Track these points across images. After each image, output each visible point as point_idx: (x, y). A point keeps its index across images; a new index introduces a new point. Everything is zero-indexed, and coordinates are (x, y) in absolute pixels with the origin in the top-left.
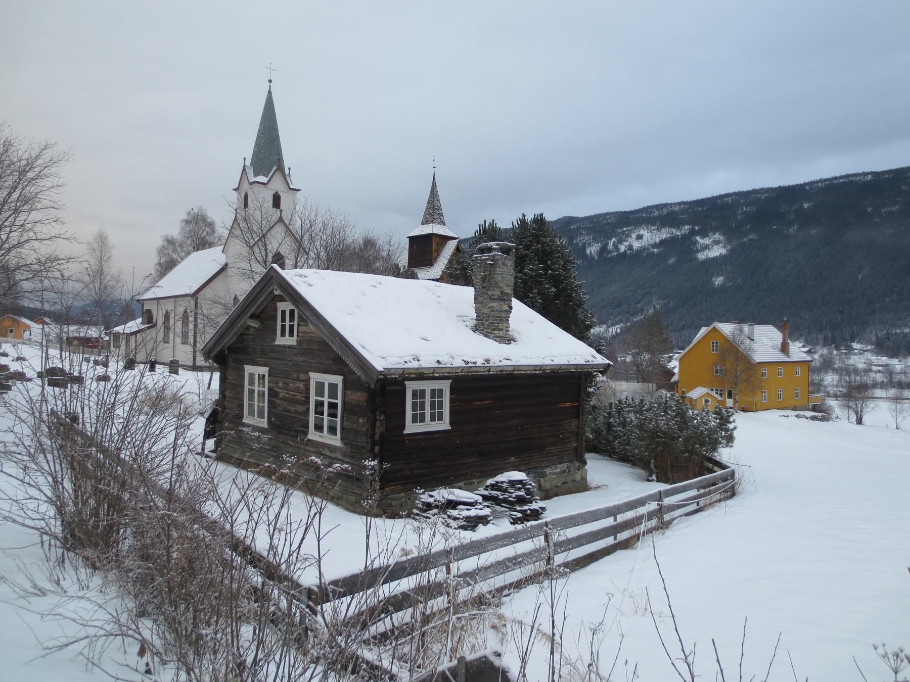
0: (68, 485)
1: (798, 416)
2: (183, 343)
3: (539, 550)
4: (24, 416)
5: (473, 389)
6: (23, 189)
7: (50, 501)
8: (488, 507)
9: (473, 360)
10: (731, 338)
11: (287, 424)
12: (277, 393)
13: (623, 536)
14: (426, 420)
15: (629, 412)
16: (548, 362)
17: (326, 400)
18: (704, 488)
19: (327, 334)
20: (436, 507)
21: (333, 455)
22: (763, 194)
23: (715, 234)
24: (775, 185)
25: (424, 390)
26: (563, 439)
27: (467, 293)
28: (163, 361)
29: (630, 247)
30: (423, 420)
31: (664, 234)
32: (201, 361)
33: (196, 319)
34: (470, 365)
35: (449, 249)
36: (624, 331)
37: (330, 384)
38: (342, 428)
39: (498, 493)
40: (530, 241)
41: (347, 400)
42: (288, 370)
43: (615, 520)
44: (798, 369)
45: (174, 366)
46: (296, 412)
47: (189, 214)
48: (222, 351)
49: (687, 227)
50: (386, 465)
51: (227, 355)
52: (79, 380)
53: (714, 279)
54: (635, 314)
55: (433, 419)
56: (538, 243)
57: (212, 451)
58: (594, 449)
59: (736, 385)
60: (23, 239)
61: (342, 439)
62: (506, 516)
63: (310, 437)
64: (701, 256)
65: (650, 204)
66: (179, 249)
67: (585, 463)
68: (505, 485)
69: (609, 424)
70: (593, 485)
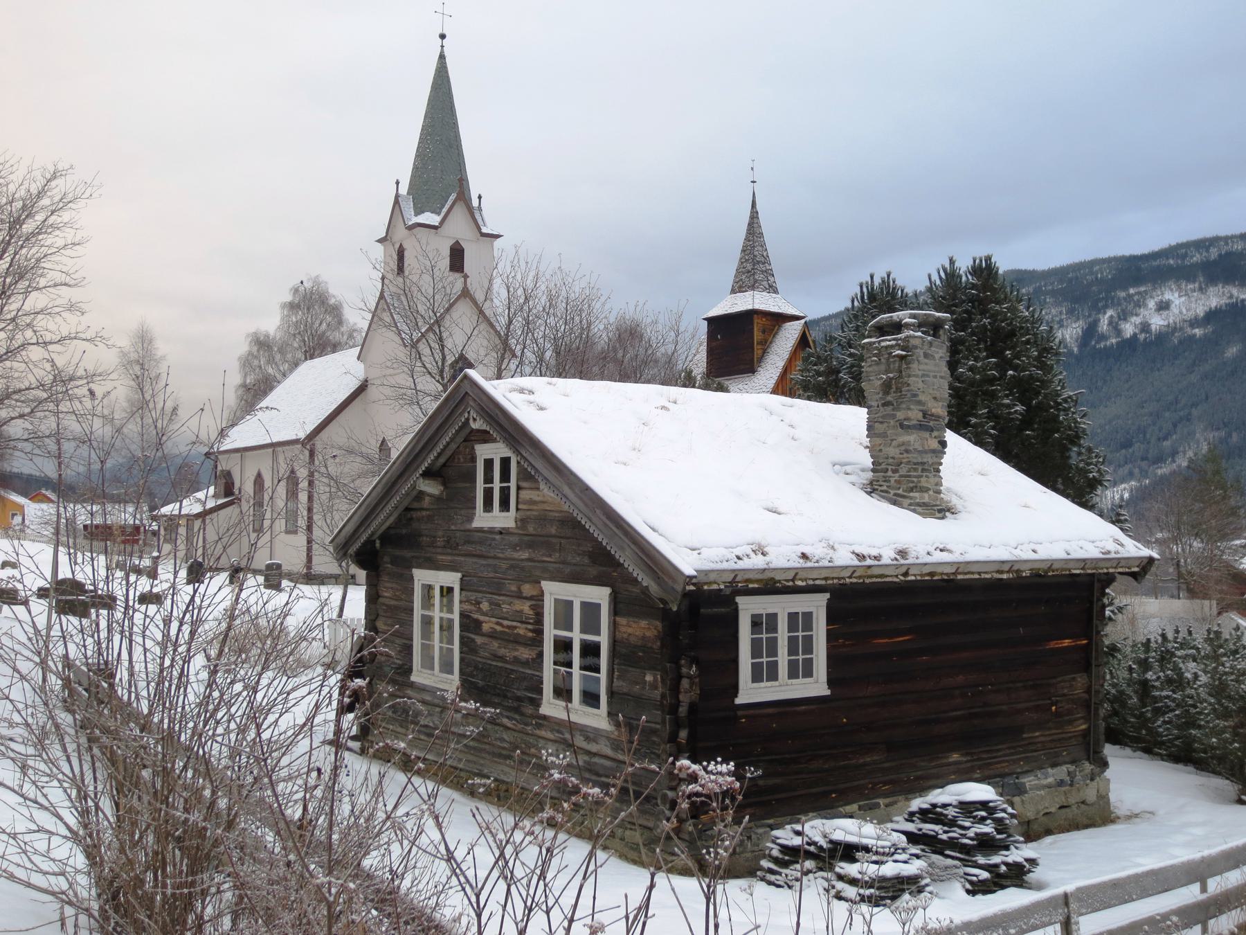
0: (106, 805)
2: (287, 532)
4: (24, 666)
5: (875, 611)
6: (16, 253)
7: (74, 837)
8: (918, 857)
9: (874, 552)
11: (500, 680)
12: (478, 624)
14: (784, 675)
15: (1185, 658)
16: (1026, 554)
17: (577, 636)
20: (809, 855)
21: (593, 748)
25: (775, 615)
26: (1057, 714)
27: (847, 423)
29: (1145, 327)
30: (773, 676)
31: (1215, 298)
32: (325, 562)
34: (869, 562)
36: (1140, 497)
38: (611, 694)
39: (937, 828)
40: (966, 311)
42: (498, 575)
43: (1204, 889)
46: (516, 661)
47: (296, 291)
48: (370, 542)
50: (751, 772)
51: (379, 552)
52: (108, 602)
54: (1159, 460)
55: (793, 674)
56: (983, 313)
57: (354, 738)
58: (1115, 737)
60: (16, 344)
61: (609, 714)
62: (955, 876)
63: (545, 710)
65: (1183, 239)
66: (278, 357)
67: (1105, 765)
68: (951, 812)
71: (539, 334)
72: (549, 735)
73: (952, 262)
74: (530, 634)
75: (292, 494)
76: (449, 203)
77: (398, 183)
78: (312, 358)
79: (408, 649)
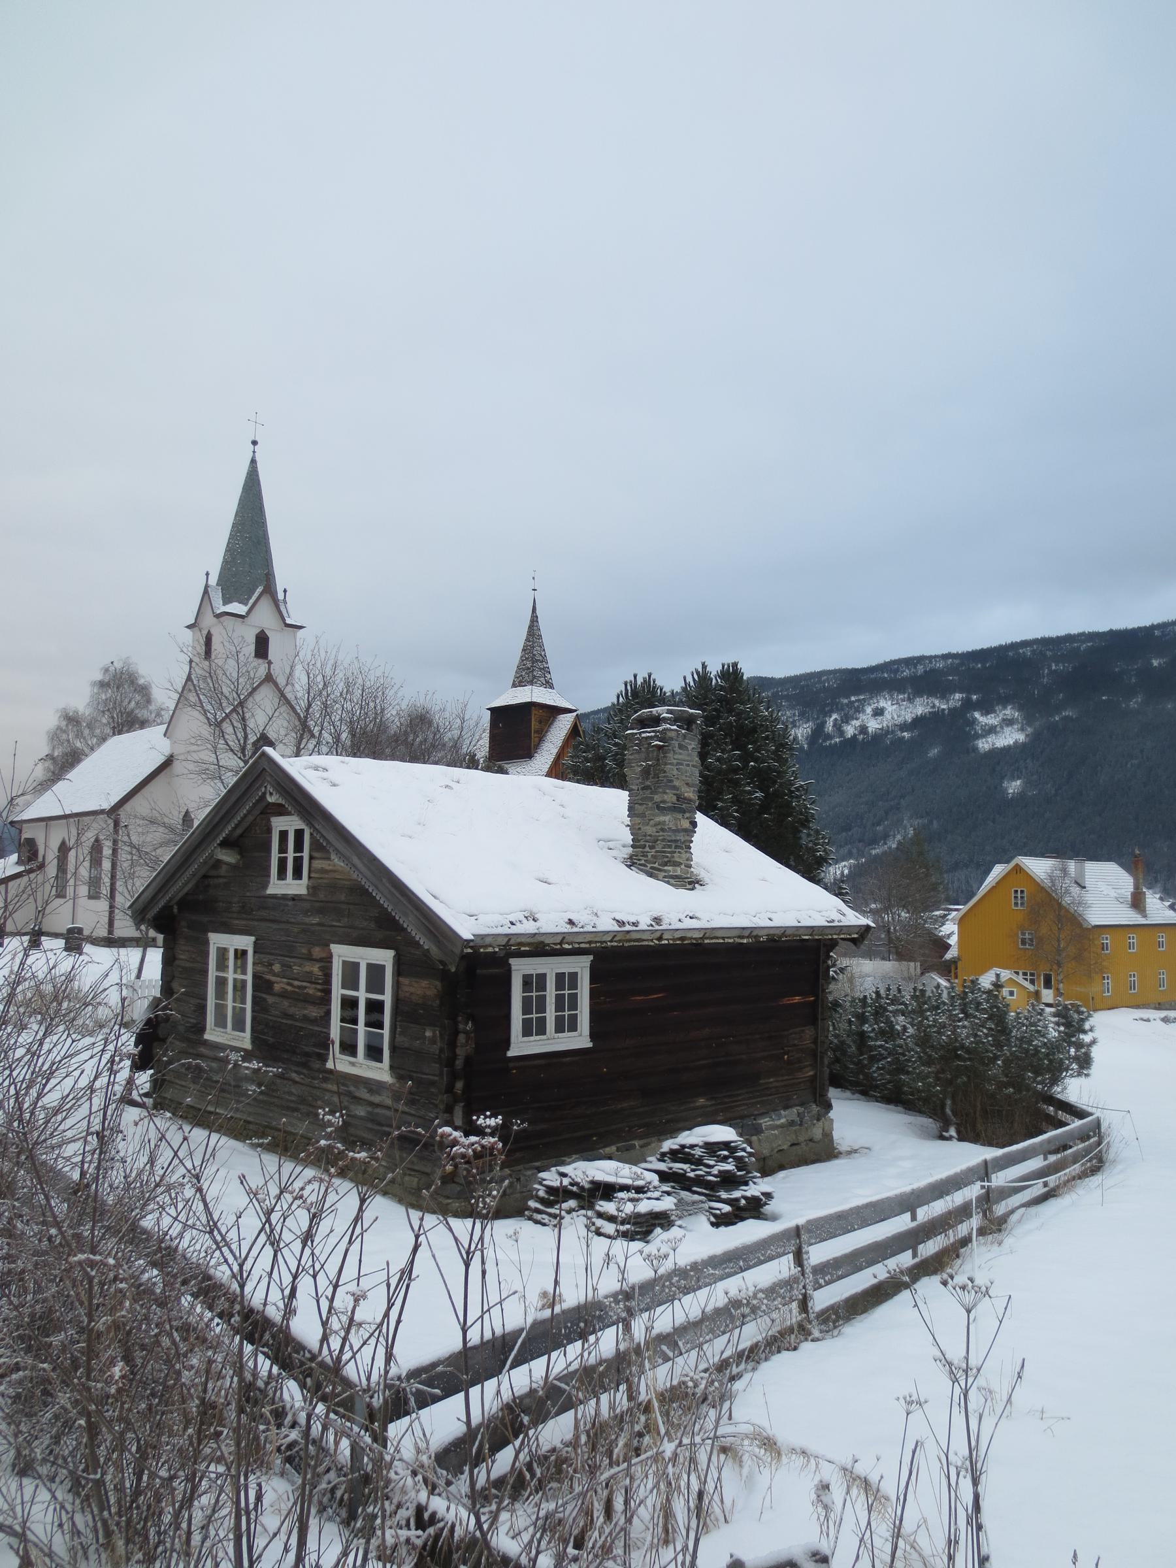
1: (1165, 1020)
2: (90, 897)
3: (788, 1283)
5: (635, 973)
8: (669, 1194)
9: (633, 920)
10: (1048, 883)
11: (290, 1037)
13: (929, 1248)
14: (551, 1031)
17: (362, 995)
18: (1056, 1151)
19: (368, 874)
21: (376, 1099)
22: (1083, 642)
23: (1005, 708)
24: (1103, 627)
25: (544, 975)
26: (789, 1062)
27: (616, 800)
28: (52, 931)
29: (863, 729)
30: (542, 1031)
31: (920, 707)
32: (125, 927)
33: (115, 851)
34: (628, 928)
35: (562, 727)
37: (370, 967)
38: (393, 1048)
39: (686, 1167)
40: (715, 710)
41: (401, 995)
42: (291, 940)
43: (914, 1218)
44: (1163, 937)
45: (74, 941)
46: (306, 1019)
47: (107, 670)
48: (167, 908)
49: (958, 696)
51: (177, 913)
53: (1005, 784)
54: (874, 842)
55: (559, 1028)
56: (730, 711)
57: (146, 1095)
58: (838, 1082)
59: (1059, 965)
61: (392, 1067)
62: (701, 1210)
64: (984, 745)
66: (86, 732)
67: (829, 1107)
68: (698, 1152)
69: (862, 1035)
70: (843, 1147)
71: (336, 717)
74: (319, 994)
75: (96, 861)
76: (256, 594)
77: (207, 574)
78: (120, 733)
79: (202, 1008)
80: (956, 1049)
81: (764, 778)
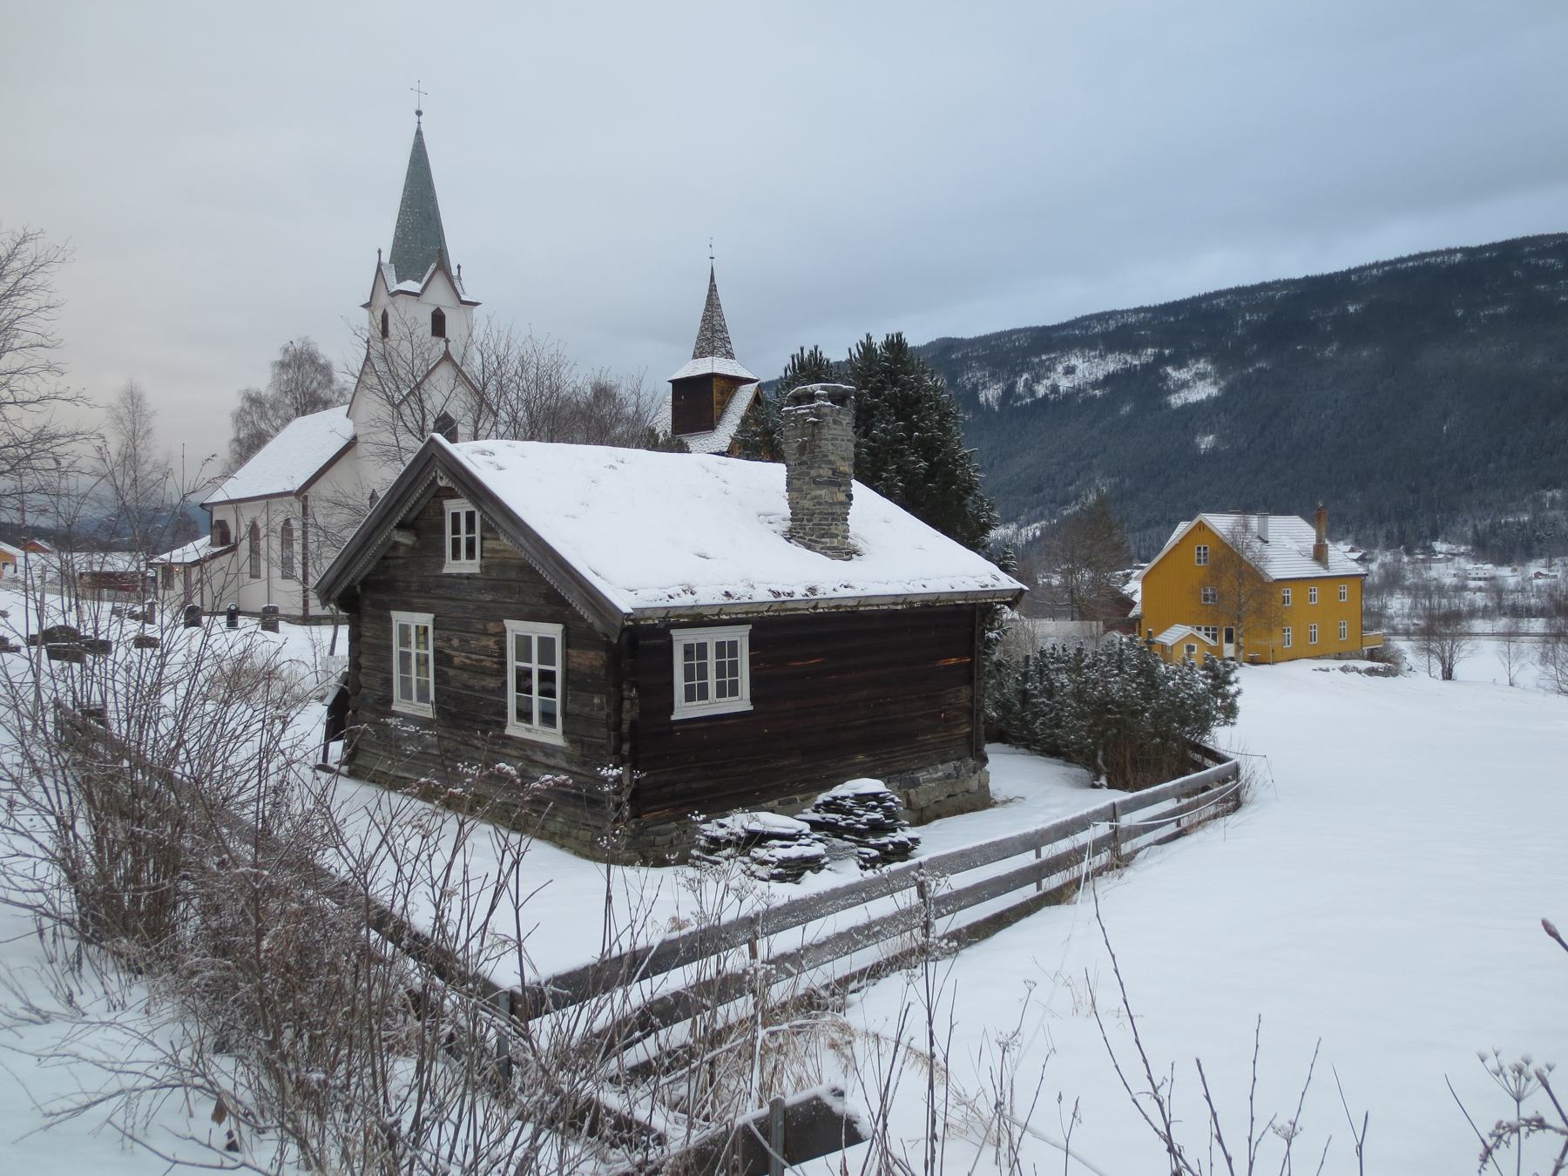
2: (284, 577)
5: (793, 641)
7: (53, 859)
8: (820, 840)
9: (788, 590)
10: (1228, 539)
11: (469, 710)
12: (450, 658)
13: (1053, 882)
14: (711, 696)
17: (535, 666)
18: (1188, 795)
22: (1277, 290)
23: (1198, 361)
24: (1298, 274)
26: (946, 720)
27: (774, 475)
28: (250, 609)
29: (1054, 388)
30: (704, 695)
31: (1112, 364)
32: (316, 608)
34: (783, 598)
36: (1048, 533)
37: (542, 640)
38: (565, 715)
39: (837, 816)
42: (467, 616)
44: (1344, 588)
45: (269, 619)
46: (484, 689)
47: (286, 350)
48: (350, 588)
49: (1150, 351)
51: (360, 594)
52: (102, 648)
53: (1198, 440)
54: (1065, 502)
56: (894, 384)
59: (1239, 619)
63: (509, 731)
64: (1176, 400)
66: (270, 413)
67: (985, 760)
68: (848, 803)
69: (1025, 692)
70: (999, 798)
71: (512, 396)
72: (514, 753)
73: (868, 336)
75: (287, 541)
76: (430, 272)
78: (304, 414)
79: (388, 682)
80: (1107, 703)
81: (928, 448)
